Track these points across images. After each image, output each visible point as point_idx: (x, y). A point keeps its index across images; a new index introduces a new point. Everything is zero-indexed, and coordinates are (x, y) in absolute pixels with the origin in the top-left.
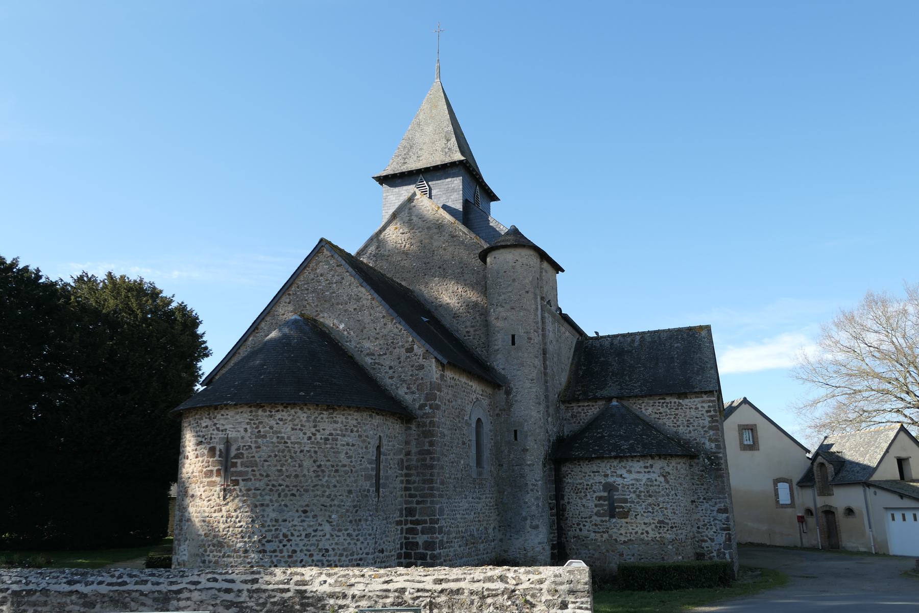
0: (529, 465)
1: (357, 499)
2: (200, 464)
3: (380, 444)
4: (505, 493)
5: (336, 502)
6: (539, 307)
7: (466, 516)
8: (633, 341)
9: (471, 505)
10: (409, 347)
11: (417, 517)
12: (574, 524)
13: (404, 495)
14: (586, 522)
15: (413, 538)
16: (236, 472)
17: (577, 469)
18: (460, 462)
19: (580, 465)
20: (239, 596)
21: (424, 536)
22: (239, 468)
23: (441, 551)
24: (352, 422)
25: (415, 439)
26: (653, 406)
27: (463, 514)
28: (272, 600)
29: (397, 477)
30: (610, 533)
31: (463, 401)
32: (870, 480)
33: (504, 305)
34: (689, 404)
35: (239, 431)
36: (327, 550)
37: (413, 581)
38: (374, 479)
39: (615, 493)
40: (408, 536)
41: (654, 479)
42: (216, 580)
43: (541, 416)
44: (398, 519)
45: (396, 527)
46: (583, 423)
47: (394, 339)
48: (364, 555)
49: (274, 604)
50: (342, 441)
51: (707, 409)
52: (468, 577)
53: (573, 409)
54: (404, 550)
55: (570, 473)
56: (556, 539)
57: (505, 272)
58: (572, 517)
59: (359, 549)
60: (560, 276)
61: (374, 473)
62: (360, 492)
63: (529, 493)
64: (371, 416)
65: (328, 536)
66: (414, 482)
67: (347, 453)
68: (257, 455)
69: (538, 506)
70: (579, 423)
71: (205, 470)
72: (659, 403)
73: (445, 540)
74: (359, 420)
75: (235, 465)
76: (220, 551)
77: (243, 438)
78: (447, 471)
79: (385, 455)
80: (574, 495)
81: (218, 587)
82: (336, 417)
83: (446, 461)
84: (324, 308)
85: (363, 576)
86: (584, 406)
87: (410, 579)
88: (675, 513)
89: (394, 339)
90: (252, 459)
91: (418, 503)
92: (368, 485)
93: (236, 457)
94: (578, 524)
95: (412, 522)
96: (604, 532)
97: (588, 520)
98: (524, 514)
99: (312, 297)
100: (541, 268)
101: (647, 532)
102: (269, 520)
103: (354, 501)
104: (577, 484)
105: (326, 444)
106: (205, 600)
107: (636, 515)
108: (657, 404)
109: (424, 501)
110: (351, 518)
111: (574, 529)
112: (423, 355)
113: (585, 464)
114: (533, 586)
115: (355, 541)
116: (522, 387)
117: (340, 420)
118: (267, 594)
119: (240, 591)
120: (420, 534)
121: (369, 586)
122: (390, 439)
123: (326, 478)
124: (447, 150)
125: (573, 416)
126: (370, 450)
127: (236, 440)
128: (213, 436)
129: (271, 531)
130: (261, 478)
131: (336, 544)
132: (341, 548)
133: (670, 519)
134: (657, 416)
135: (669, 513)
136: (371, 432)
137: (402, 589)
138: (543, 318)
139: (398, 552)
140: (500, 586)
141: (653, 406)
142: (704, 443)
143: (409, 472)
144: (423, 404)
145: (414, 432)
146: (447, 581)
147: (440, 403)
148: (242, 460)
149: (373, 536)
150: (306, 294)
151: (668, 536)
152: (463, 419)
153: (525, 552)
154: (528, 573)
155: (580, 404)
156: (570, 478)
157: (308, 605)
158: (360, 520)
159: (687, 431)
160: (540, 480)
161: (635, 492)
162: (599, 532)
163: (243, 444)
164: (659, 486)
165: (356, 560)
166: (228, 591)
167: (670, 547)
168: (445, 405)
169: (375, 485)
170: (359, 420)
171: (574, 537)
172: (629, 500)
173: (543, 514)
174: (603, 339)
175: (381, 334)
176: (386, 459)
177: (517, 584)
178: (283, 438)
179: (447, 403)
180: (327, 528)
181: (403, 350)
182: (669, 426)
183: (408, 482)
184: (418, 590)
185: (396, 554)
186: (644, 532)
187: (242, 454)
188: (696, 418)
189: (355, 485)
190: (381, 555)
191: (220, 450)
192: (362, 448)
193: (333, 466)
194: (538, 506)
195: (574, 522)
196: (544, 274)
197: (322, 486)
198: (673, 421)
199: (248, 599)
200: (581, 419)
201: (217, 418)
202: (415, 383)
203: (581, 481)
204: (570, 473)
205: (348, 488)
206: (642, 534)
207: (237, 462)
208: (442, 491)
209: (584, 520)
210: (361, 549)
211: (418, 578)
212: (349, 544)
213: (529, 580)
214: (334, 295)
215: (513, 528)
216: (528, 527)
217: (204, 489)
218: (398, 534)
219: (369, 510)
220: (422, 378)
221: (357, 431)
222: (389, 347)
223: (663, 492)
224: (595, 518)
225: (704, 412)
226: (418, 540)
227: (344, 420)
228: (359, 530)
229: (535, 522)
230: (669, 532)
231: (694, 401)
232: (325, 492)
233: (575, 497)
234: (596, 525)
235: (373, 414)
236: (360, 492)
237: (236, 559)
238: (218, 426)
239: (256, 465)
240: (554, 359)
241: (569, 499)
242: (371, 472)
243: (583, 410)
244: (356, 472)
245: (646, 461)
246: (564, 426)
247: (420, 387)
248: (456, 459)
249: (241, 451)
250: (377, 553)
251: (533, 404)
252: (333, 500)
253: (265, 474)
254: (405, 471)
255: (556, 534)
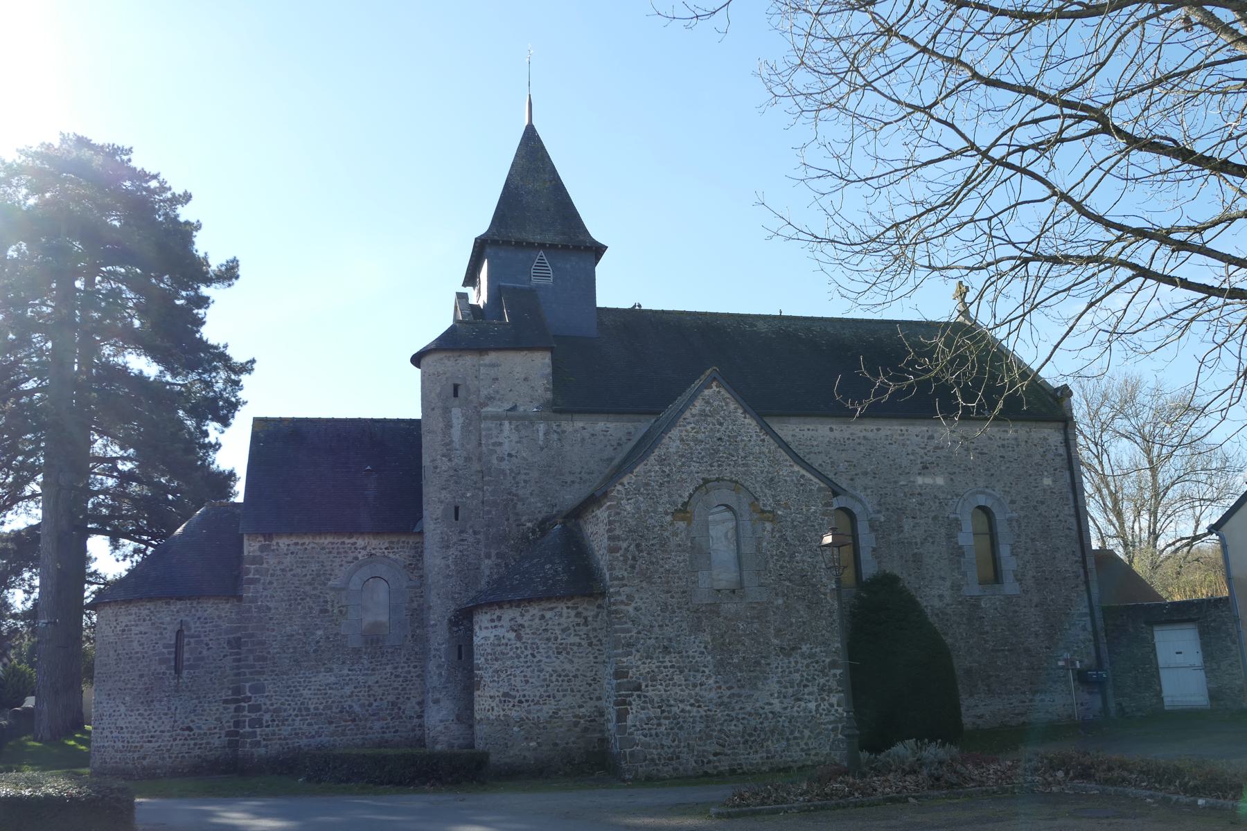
5: (129, 686)
32: (363, 627)
36: (122, 728)
41: (501, 636)
50: (135, 630)
61: (173, 656)
64: (167, 603)
65: (123, 716)
67: (139, 641)
74: (152, 609)
88: (527, 682)
105: (123, 635)
110: (142, 700)
117: (133, 612)
123: (122, 665)
131: (129, 723)
132: (133, 726)
133: (518, 691)
135: (518, 682)
151: (514, 714)
164: (507, 645)
165: (147, 737)
167: (516, 729)
170: (152, 609)
180: (123, 709)
192: (156, 635)
193: (127, 654)
194: (440, 675)
197: (120, 672)
205: (140, 673)
212: (140, 722)
219: (164, 691)
223: (511, 654)
229: (437, 695)
230: (516, 708)
232: (121, 677)
245: (493, 612)
251: (438, 549)
252: (126, 684)
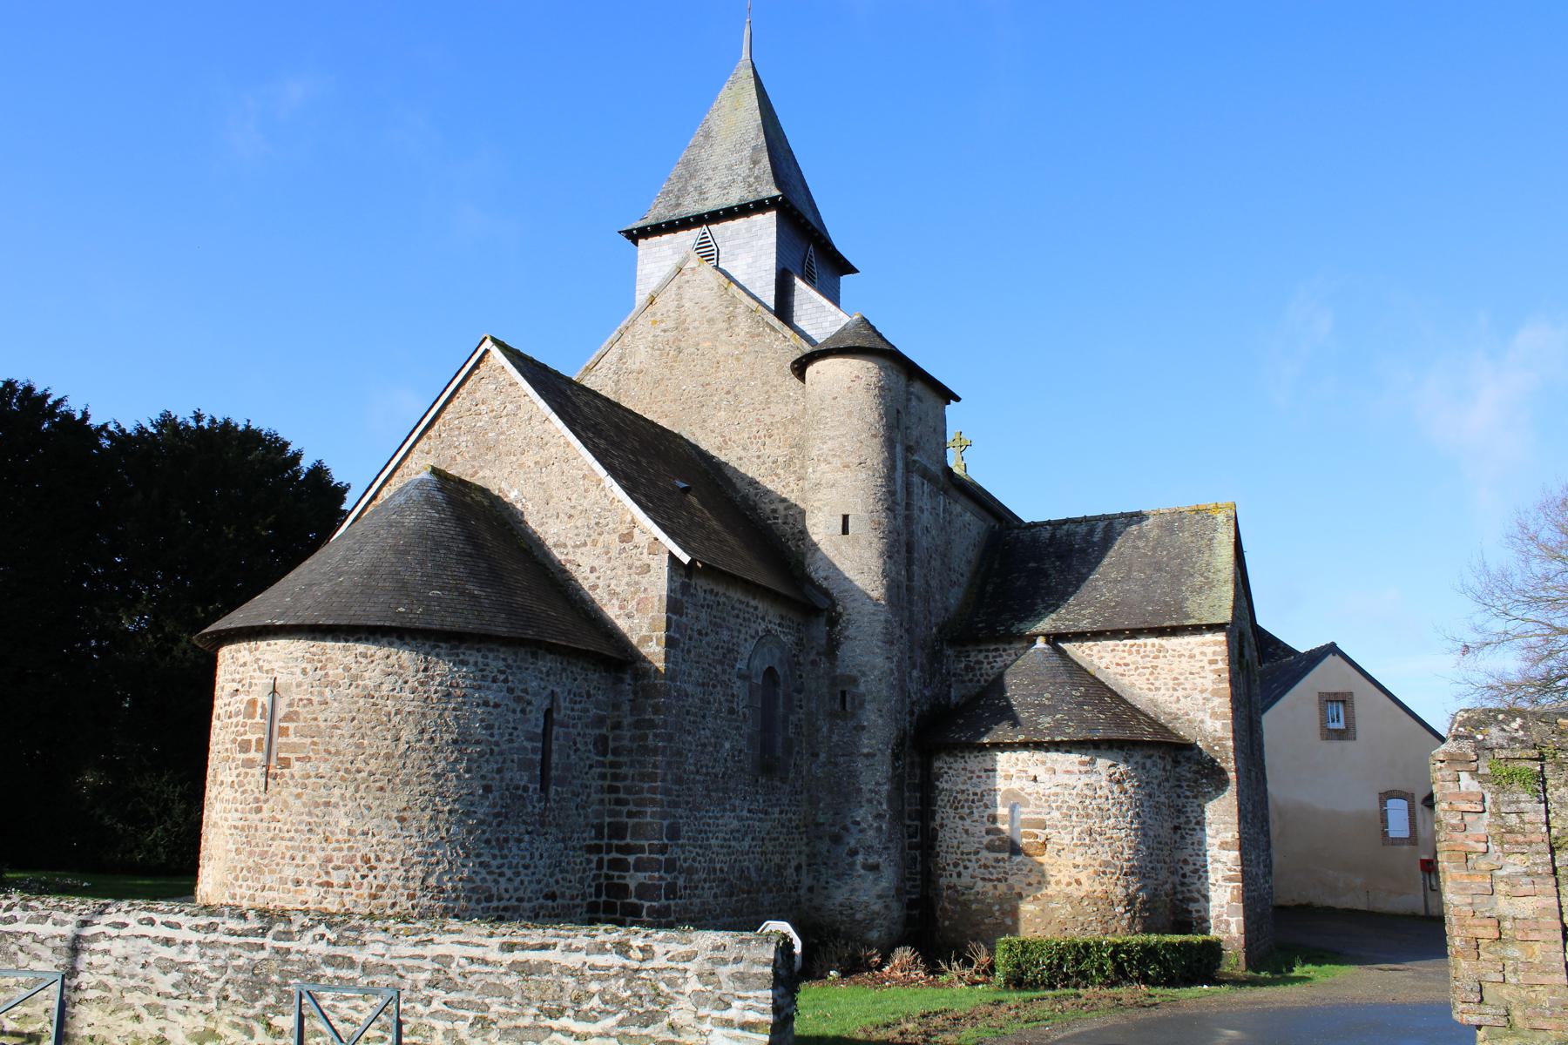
0: (867, 756)
1: (500, 802)
2: (233, 728)
3: (552, 703)
4: (821, 805)
6: (900, 465)
7: (733, 843)
8: (1091, 532)
9: (746, 823)
10: (626, 532)
11: (628, 840)
12: (948, 865)
13: (607, 800)
14: (970, 861)
15: (619, 877)
16: (285, 744)
17: (959, 765)
18: (722, 746)
19: (963, 757)
20: (184, 953)
21: (639, 874)
22: (293, 739)
23: (672, 903)
24: (495, 663)
25: (630, 701)
26: (1113, 650)
27: (725, 839)
28: (235, 963)
29: (591, 767)
30: (1010, 881)
31: (735, 634)
33: (830, 458)
34: (1178, 648)
35: (292, 673)
37: (466, 944)
38: (539, 769)
39: (1022, 809)
40: (611, 873)
42: (152, 922)
43: (893, 666)
44: (593, 842)
45: (587, 856)
46: (986, 681)
47: (600, 517)
48: (514, 903)
49: (238, 969)
51: (1210, 656)
52: (561, 943)
53: (968, 656)
54: (604, 898)
55: (946, 773)
56: (918, 890)
57: (835, 398)
58: (947, 852)
59: (502, 891)
60: (951, 409)
62: (507, 789)
63: (862, 806)
66: (625, 778)
68: (321, 717)
69: (879, 829)
70: (979, 681)
71: (239, 739)
72: (1125, 645)
73: (681, 882)
74: (510, 661)
75: (284, 732)
76: (258, 880)
77: (299, 685)
78: (691, 761)
79: (562, 725)
80: (951, 812)
81: (153, 935)
82: (464, 654)
83: (690, 743)
84: (485, 461)
85: (386, 930)
86: (987, 651)
87: (461, 940)
89: (600, 517)
90: (312, 723)
91: (630, 815)
92: (525, 778)
93: (288, 718)
94: (956, 865)
95: (620, 849)
96: (999, 880)
97: (973, 858)
98: (853, 843)
99: (467, 441)
100: (909, 393)
101: (1078, 882)
102: (338, 831)
103: (494, 805)
104: (957, 793)
106: (132, 956)
107: (1059, 851)
108: (1121, 648)
109: (640, 812)
111: (948, 873)
112: (649, 547)
113: (972, 756)
114: (673, 964)
115: (496, 876)
116: (859, 612)
117: (472, 660)
118: (227, 952)
119: (185, 944)
120: (632, 871)
121: (393, 948)
122: (578, 699)
124: (752, 180)
125: (968, 668)
126: (532, 716)
127: (288, 688)
128: (253, 681)
129: (341, 850)
130: (327, 756)
134: (1120, 670)
136: (534, 684)
137: (446, 956)
138: (908, 487)
139: (589, 900)
140: (615, 960)
141: (1113, 650)
142: (1202, 722)
143: (617, 759)
144: (645, 636)
145: (628, 687)
146: (524, 947)
147: (677, 636)
148: (295, 724)
149: (532, 870)
150: (456, 436)
152: (733, 667)
153: (850, 911)
154: (666, 940)
155: (983, 647)
156: (947, 782)
157: (292, 974)
158: (506, 840)
159: (1174, 699)
160: (885, 783)
161: (1058, 808)
162: (991, 880)
163: (299, 697)
165: (496, 909)
166: (168, 942)
168: (690, 639)
169: (539, 779)
170: (510, 661)
171: (949, 887)
172: (1048, 823)
173: (890, 845)
174: (1038, 528)
175: (580, 508)
176: (567, 735)
177: (643, 960)
178: (365, 687)
179: (696, 635)
181: (616, 537)
182: (1141, 689)
183: (615, 777)
184: (472, 960)
185: (585, 903)
186: (1073, 881)
187: (296, 713)
188: (1191, 673)
189: (497, 777)
190: (550, 903)
191: (263, 706)
192: (514, 711)
195: (949, 861)
196: (914, 402)
198: (1148, 679)
199: (197, 958)
200: (981, 675)
201: (261, 649)
202: (633, 599)
203: (964, 787)
204: (946, 773)
206: (1069, 884)
207: (287, 728)
208: (678, 796)
209: (965, 857)
210: (507, 891)
211: (476, 940)
213: (668, 952)
214: (503, 437)
215: (832, 868)
216: (859, 867)
217: (238, 771)
218: (591, 869)
219: (525, 822)
220: (645, 590)
221: (506, 681)
222: (591, 532)
224: (984, 853)
225: (1205, 663)
226: (628, 881)
227: (480, 660)
228: (505, 857)
231: (1189, 643)
233: (953, 815)
234: (986, 867)
235: (540, 652)
236: (507, 789)
237: (282, 895)
238: (261, 663)
239: (320, 734)
240: (933, 563)
241: (942, 818)
242: (530, 756)
243: (987, 657)
244: (501, 753)
246: (950, 686)
247: (642, 605)
248: (713, 740)
249: (295, 708)
250: (541, 900)
251: (880, 644)
253: (333, 750)
254: (610, 757)
255: (918, 882)
